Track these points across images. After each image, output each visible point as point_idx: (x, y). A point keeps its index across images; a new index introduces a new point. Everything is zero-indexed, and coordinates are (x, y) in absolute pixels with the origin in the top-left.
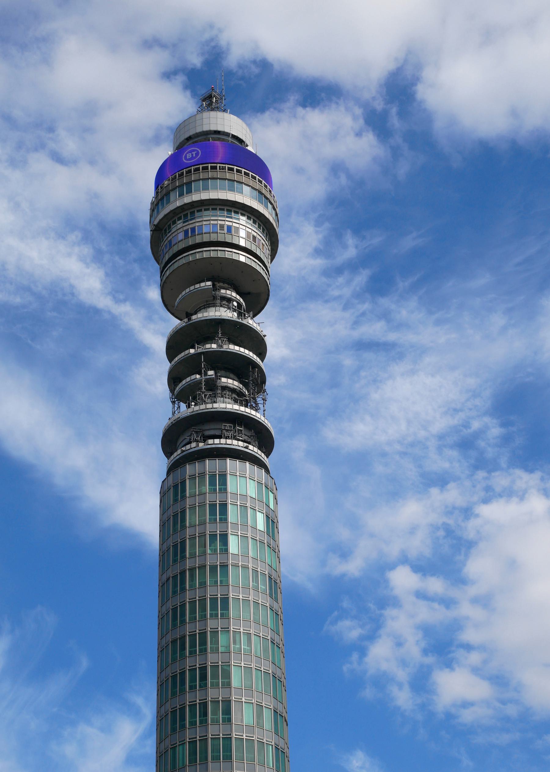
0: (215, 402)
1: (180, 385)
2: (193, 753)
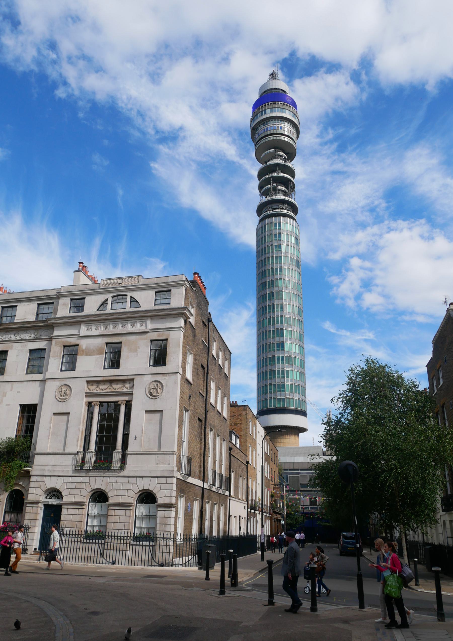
2: (270, 322)
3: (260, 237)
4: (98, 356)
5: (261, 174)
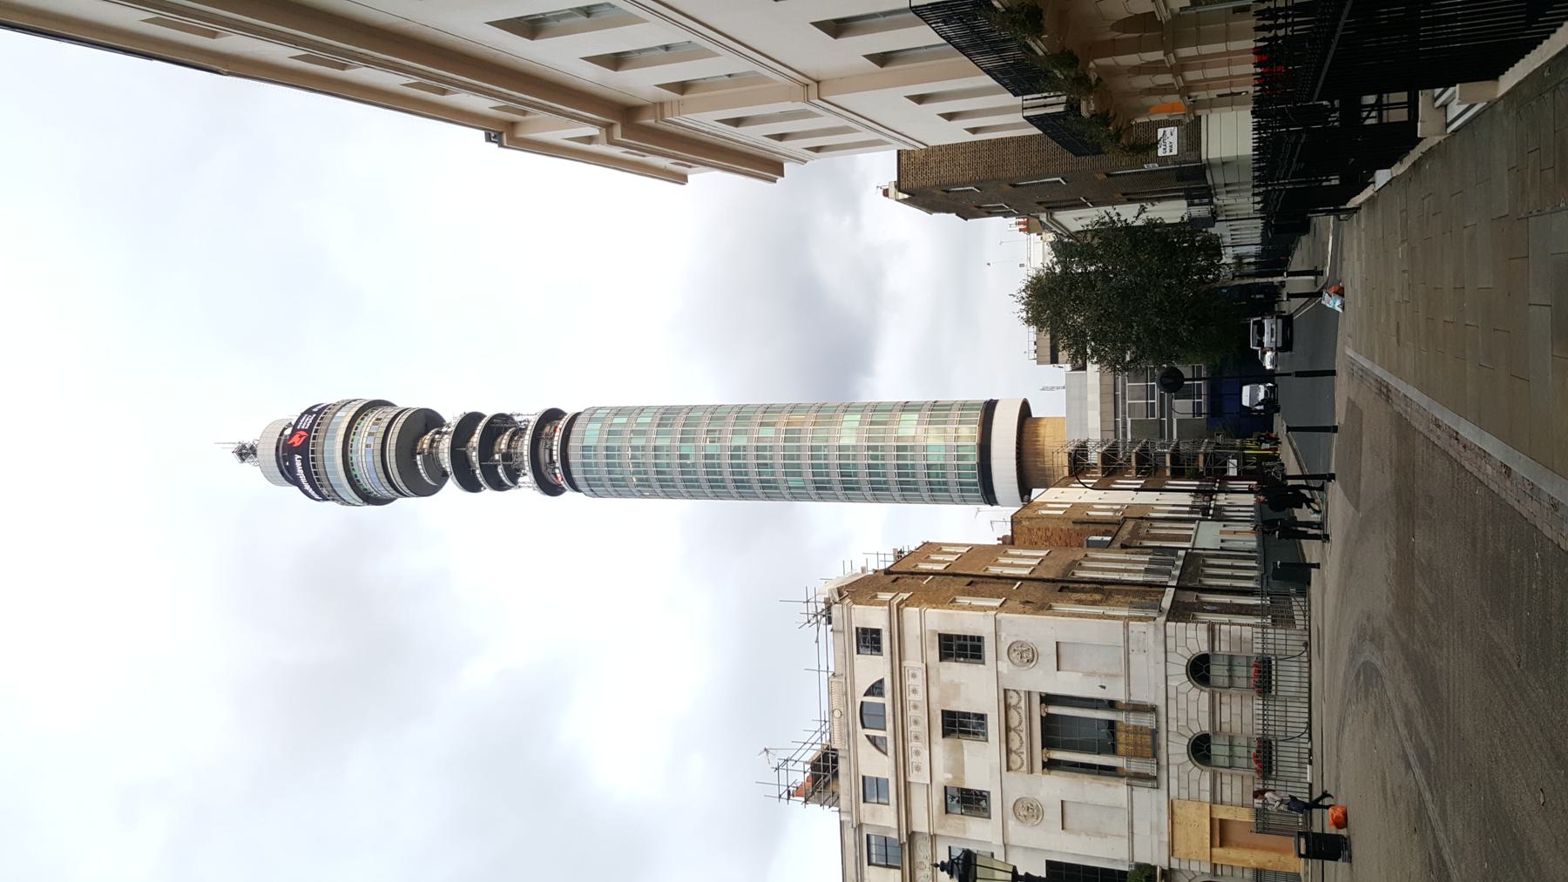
0: (522, 454)
1: (506, 481)
2: (794, 474)
3: (611, 489)
4: (965, 752)
5: (470, 485)
